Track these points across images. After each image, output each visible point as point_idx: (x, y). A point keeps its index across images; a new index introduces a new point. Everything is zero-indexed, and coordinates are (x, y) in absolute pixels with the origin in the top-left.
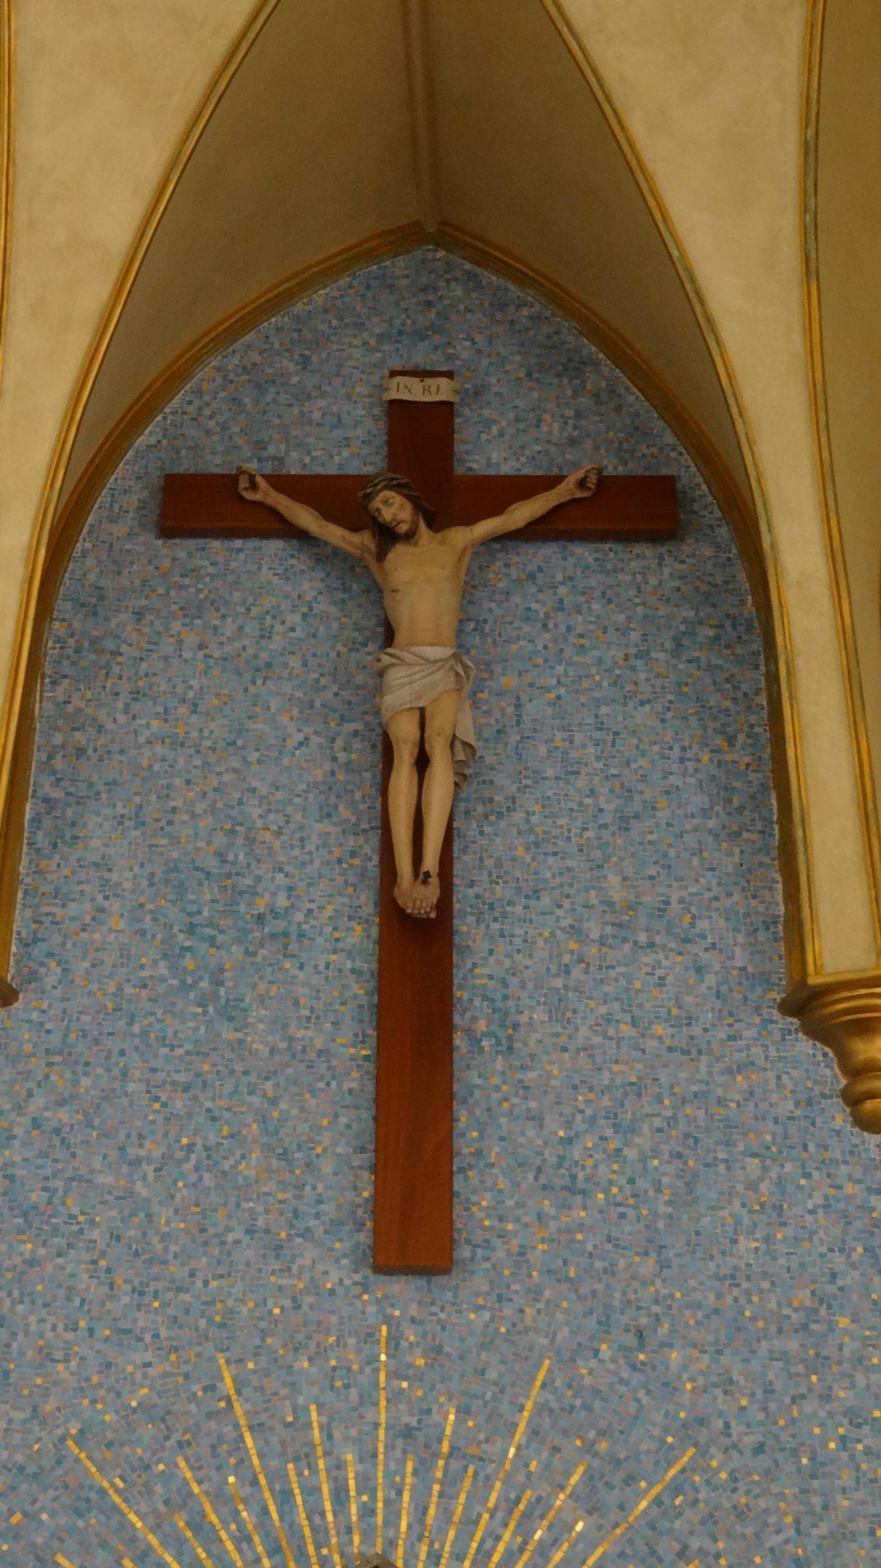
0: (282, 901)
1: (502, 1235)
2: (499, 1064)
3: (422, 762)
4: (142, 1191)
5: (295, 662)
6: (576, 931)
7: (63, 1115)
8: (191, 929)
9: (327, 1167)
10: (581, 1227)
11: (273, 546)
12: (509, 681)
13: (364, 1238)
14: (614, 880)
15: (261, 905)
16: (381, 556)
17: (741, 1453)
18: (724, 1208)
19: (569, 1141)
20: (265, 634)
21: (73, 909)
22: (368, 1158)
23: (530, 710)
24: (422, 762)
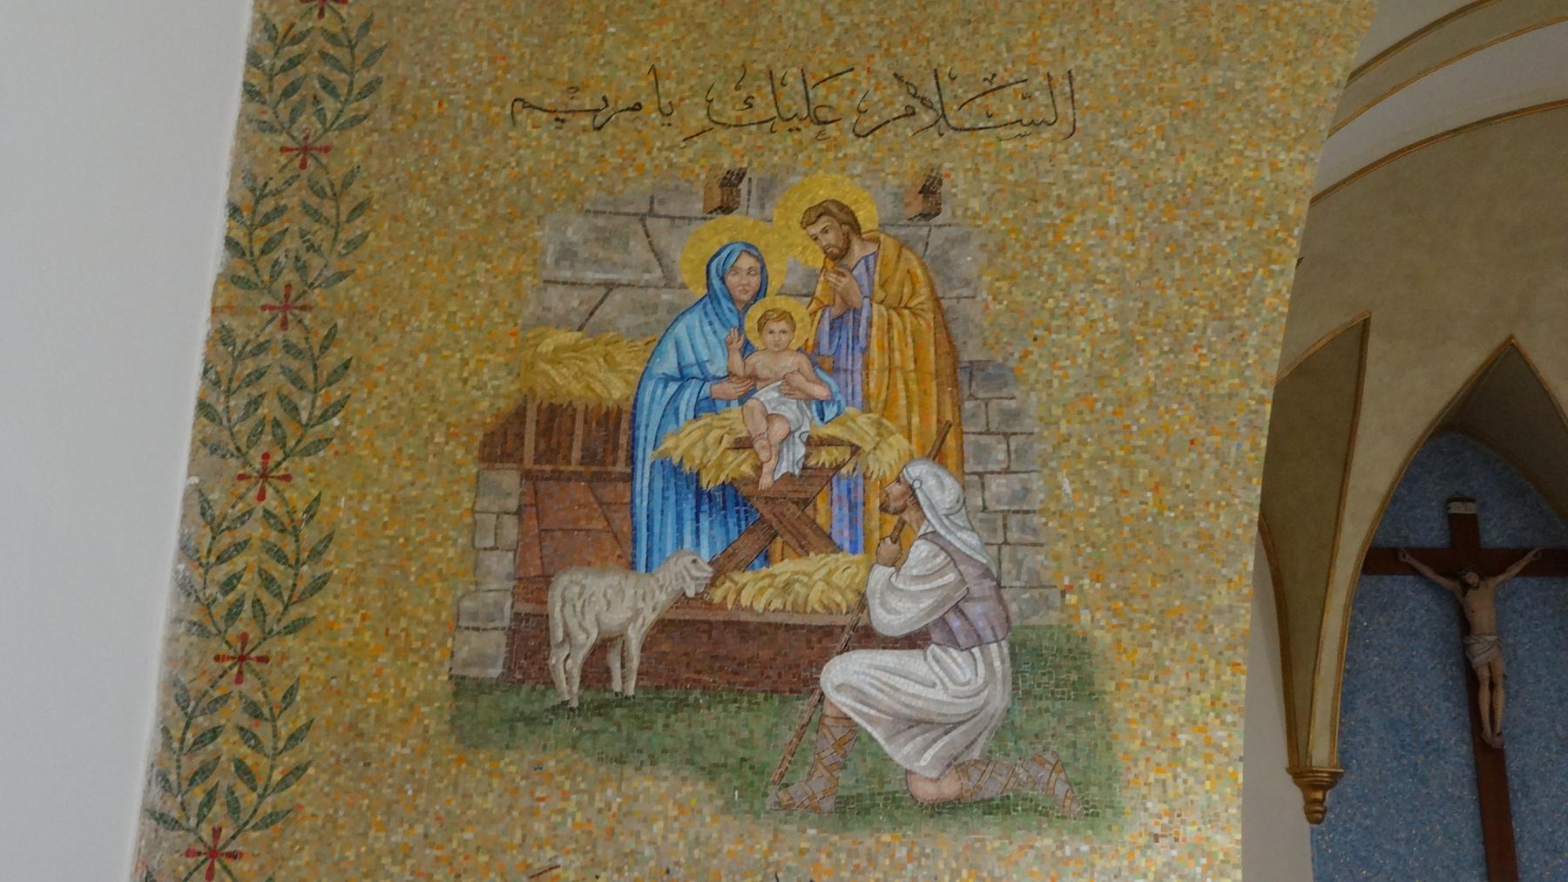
0: (1436, 736)
1: (1533, 869)
2: (1524, 802)
3: (1492, 686)
4: (1401, 851)
5: (1425, 631)
6: (1547, 748)
7: (1368, 822)
8: (1403, 747)
9: (1467, 843)
10: (1560, 865)
11: (1410, 578)
12: (1510, 641)
13: (1483, 870)
14: (1559, 728)
15: (1427, 737)
16: (1464, 594)
17: (397, 802)
18: (324, 31)
19: (1553, 833)
20: (1413, 619)
21: (1358, 739)
22: (1481, 839)
23: (1520, 652)
24: (1492, 686)
